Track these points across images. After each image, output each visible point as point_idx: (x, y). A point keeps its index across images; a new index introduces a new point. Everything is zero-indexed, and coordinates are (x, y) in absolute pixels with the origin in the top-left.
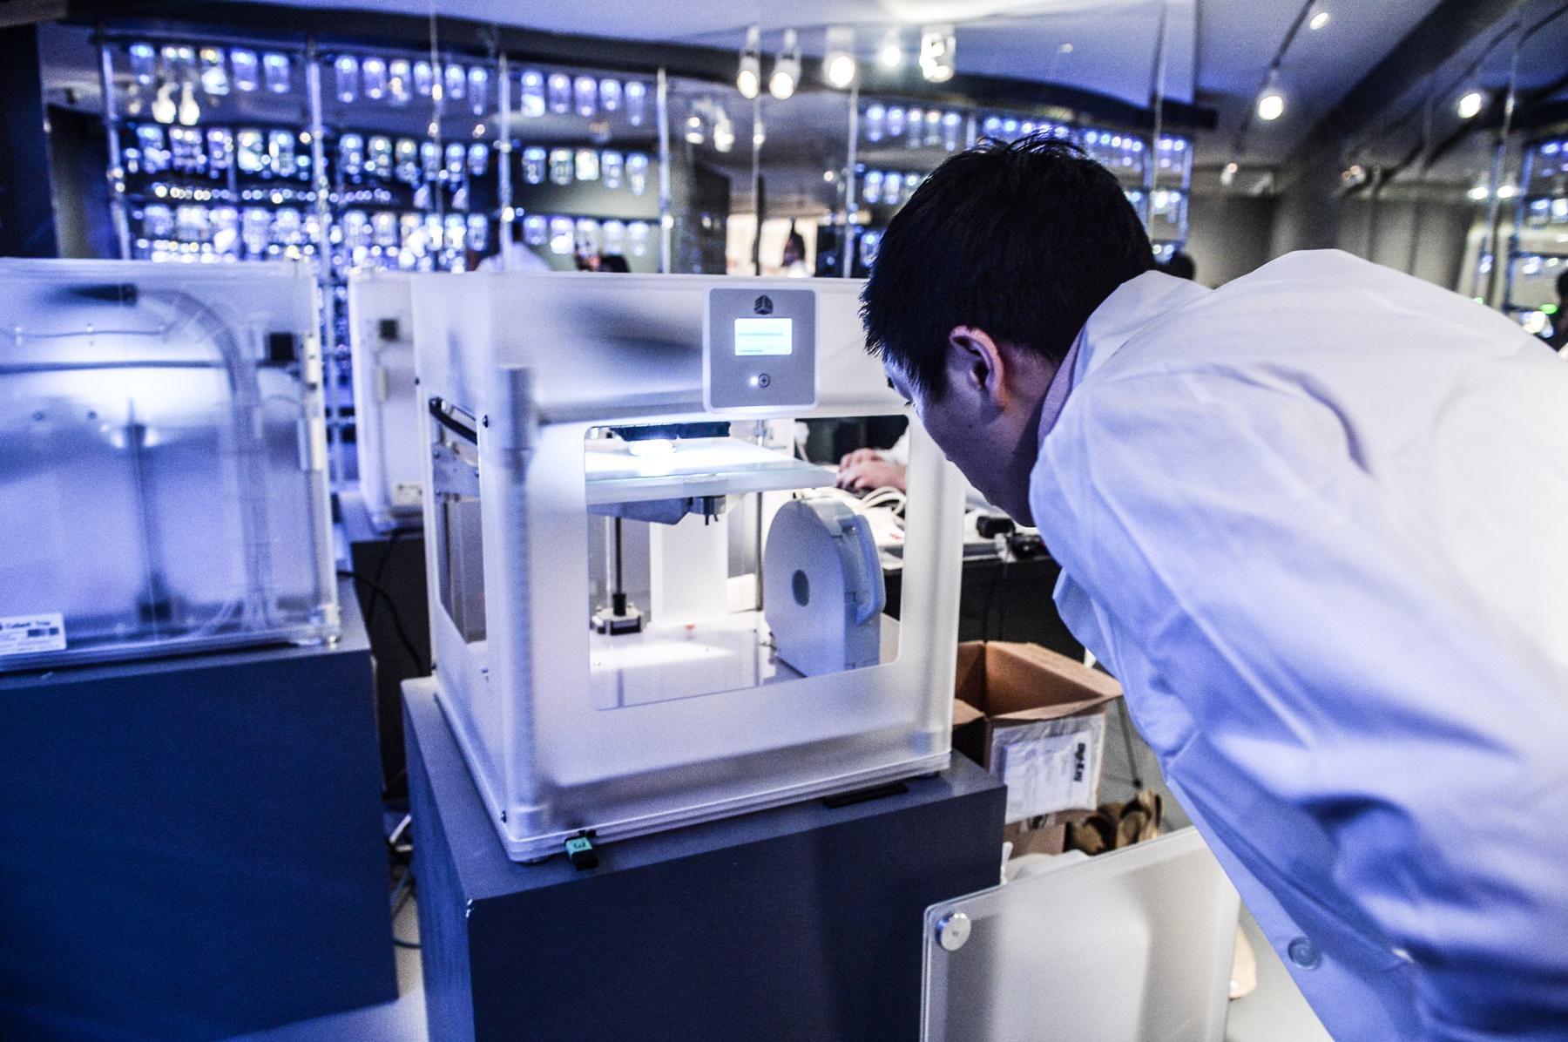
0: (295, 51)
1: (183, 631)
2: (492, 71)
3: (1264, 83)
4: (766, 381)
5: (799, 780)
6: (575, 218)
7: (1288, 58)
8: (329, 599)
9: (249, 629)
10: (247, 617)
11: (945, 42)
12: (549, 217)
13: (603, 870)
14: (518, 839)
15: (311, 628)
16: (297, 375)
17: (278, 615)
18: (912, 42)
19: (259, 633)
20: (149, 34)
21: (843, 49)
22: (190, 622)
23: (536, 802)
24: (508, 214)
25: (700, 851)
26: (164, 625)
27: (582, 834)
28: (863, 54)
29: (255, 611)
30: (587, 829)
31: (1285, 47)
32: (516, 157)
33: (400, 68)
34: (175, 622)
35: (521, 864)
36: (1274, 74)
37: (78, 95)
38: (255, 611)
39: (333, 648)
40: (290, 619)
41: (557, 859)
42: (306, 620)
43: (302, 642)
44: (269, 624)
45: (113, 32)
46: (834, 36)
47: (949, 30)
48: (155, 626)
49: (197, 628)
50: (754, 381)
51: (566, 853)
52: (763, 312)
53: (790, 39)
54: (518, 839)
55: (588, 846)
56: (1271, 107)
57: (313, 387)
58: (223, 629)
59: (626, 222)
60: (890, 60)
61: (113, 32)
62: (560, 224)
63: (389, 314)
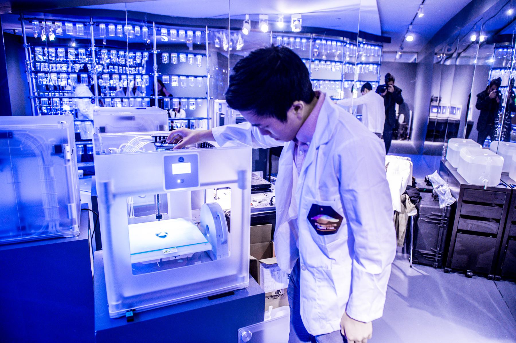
0: (86, 22)
1: (31, 234)
2: (150, 28)
3: (408, 31)
4: (183, 181)
5: (431, 146)
6: (179, 76)
7: (414, 23)
8: (75, 224)
9: (51, 233)
10: (50, 229)
11: (299, 21)
12: (170, 75)
13: (137, 321)
14: (113, 312)
15: (70, 232)
16: (63, 157)
17: (59, 228)
18: (288, 20)
19: (55, 234)
20: (38, 17)
21: (265, 21)
22: (33, 231)
23: (118, 301)
24: (156, 75)
25: (161, 316)
26: (24, 233)
27: (131, 310)
28: (271, 22)
29: (52, 227)
30: (133, 309)
31: (414, 19)
32: (159, 56)
33: (120, 27)
34: (28, 232)
35: (114, 319)
36: (411, 27)
37: (16, 31)
38: (52, 227)
39: (77, 238)
40: (63, 230)
41: (122, 317)
42: (69, 230)
43: (67, 237)
44: (57, 231)
45: (26, 17)
46: (261, 17)
47: (300, 16)
48: (21, 233)
49: (34, 233)
50: (179, 181)
51: (125, 316)
52: (181, 162)
53: (247, 17)
54: (113, 312)
55: (132, 315)
56: (410, 38)
57: (69, 160)
58: (43, 233)
59: (196, 77)
60: (281, 25)
61: (26, 17)
62: (174, 78)
63: (102, 126)
